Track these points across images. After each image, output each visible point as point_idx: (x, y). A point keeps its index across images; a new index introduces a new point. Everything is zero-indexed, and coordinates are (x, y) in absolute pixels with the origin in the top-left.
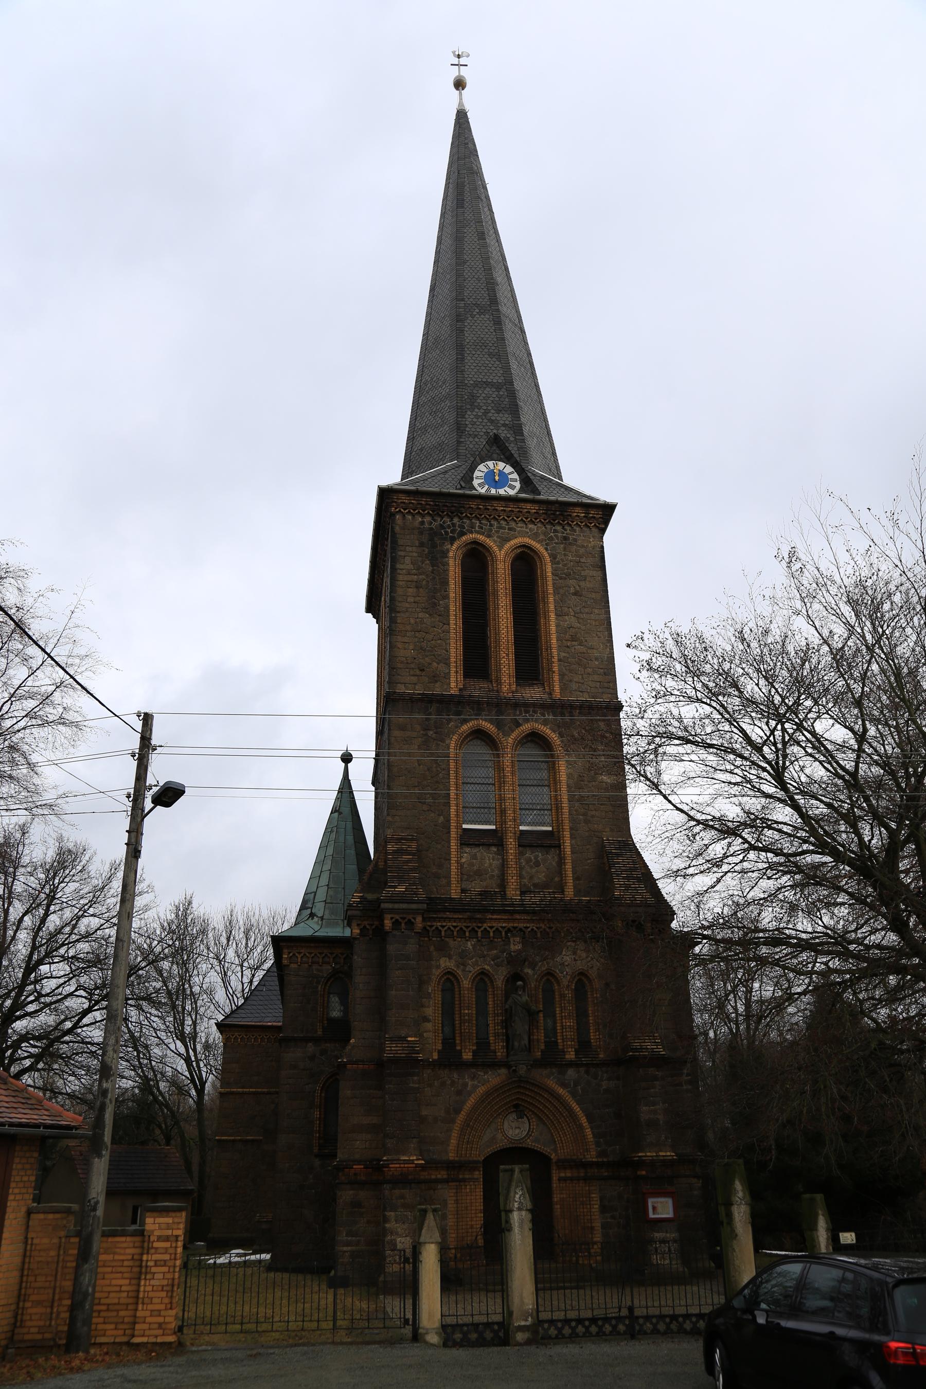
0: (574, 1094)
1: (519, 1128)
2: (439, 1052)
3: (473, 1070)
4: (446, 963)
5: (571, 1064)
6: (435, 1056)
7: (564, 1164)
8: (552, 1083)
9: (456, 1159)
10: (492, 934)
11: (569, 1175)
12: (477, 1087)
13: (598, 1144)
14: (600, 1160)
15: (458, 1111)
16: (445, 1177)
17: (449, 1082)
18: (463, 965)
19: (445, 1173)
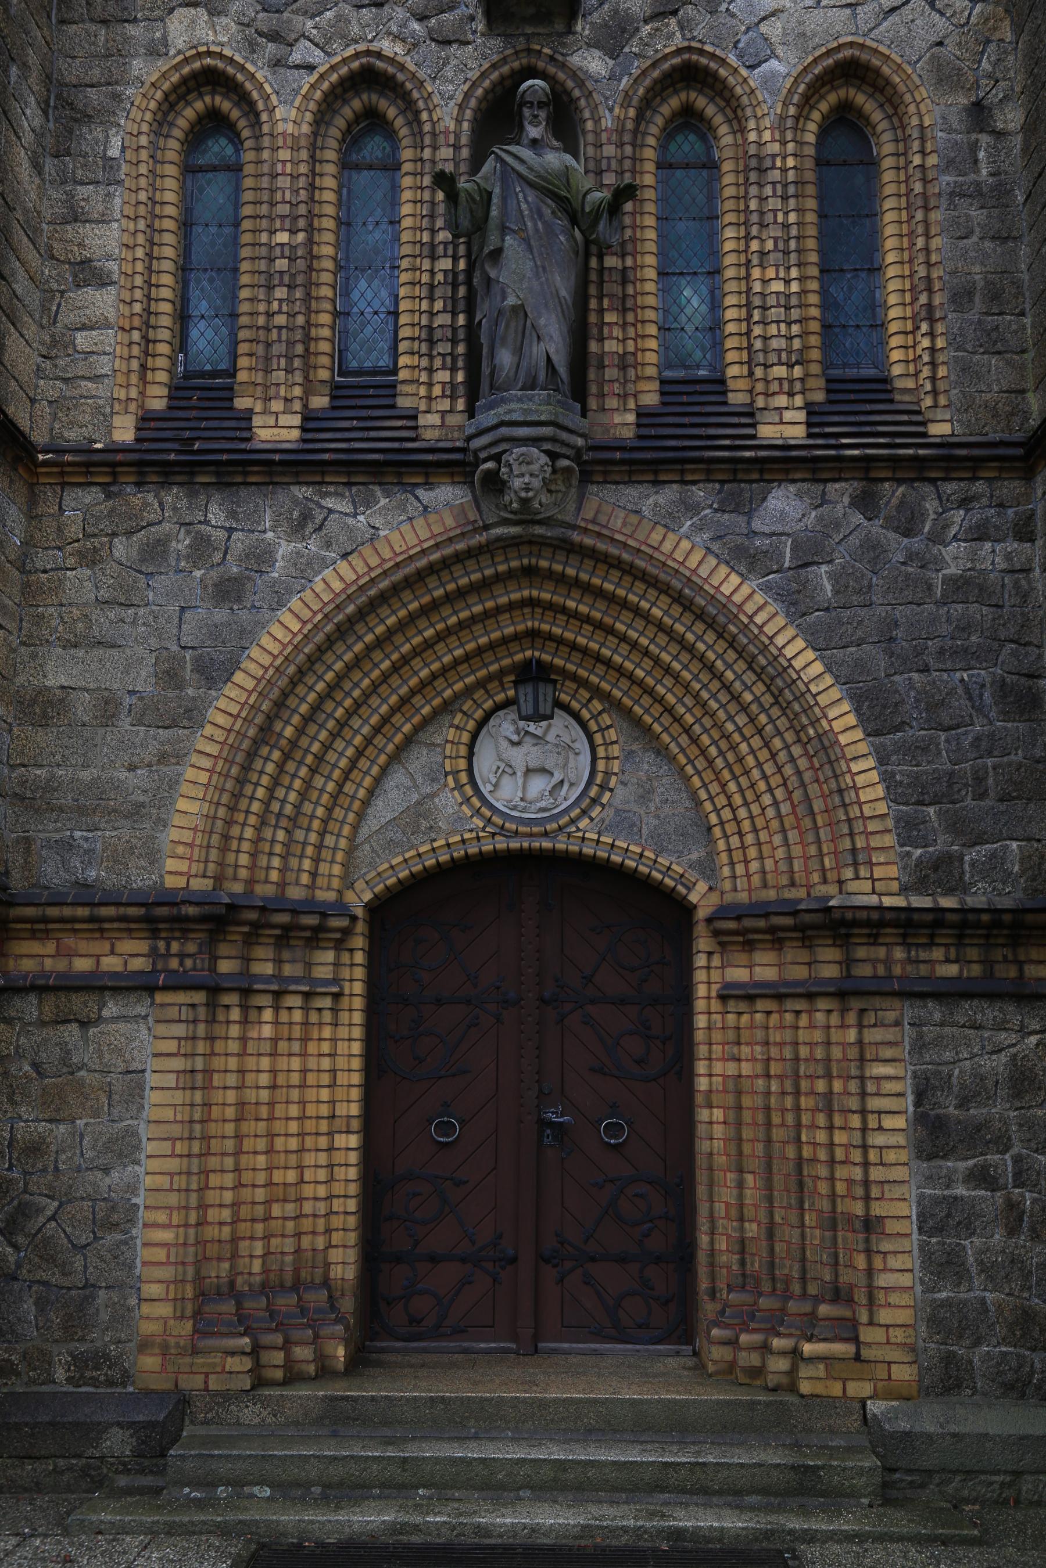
0: (795, 602)
1: (543, 771)
2: (146, 419)
3: (302, 492)
5: (782, 465)
6: (124, 431)
7: (747, 927)
9: (199, 884)
11: (767, 973)
13: (909, 830)
14: (920, 902)
15: (215, 672)
16: (138, 964)
17: (182, 543)
18: (274, 37)
19: (142, 946)
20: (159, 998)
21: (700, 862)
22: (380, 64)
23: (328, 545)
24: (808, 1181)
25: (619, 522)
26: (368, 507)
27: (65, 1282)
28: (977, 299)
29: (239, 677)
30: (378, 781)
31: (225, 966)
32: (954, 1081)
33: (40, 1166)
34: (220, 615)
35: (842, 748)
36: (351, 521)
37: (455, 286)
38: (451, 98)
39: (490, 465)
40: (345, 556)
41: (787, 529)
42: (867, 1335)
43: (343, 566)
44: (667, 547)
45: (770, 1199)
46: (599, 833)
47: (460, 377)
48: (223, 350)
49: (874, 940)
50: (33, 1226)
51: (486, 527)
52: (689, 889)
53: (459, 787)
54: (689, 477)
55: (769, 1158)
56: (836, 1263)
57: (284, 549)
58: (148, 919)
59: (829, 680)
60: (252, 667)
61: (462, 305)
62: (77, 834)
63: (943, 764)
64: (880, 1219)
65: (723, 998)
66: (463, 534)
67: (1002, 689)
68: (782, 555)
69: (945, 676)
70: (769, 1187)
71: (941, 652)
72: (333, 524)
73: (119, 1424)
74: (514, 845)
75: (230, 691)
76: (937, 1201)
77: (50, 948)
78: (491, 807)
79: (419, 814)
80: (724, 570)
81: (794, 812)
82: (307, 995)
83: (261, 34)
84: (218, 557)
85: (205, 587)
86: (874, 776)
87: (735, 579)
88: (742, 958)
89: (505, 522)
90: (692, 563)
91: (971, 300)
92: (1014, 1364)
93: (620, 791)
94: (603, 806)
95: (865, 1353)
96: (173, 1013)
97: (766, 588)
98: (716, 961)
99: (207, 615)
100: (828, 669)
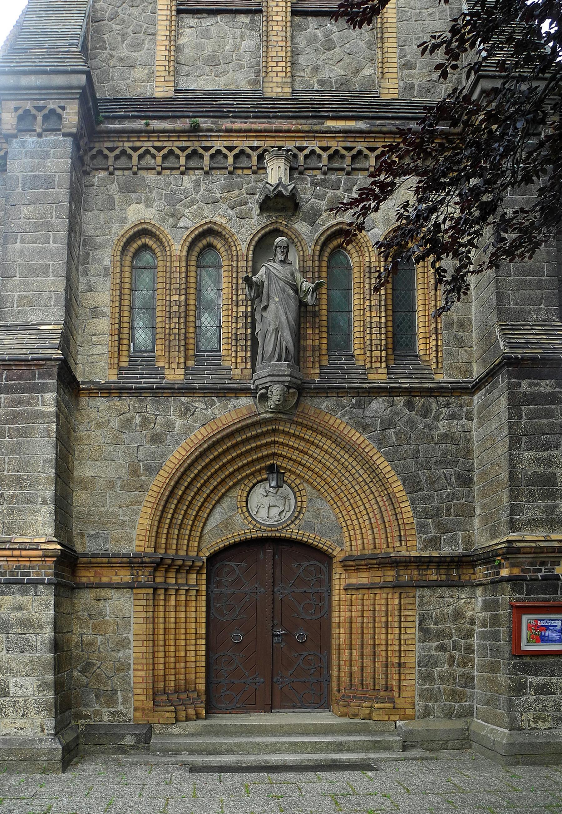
0: (380, 442)
4: (137, 213)
7: (353, 564)
8: (339, 422)
10: (231, 160)
12: (191, 429)
14: (426, 554)
17: (138, 420)
18: (173, 216)
20: (135, 591)
21: (338, 540)
22: (215, 227)
23: (196, 421)
24: (377, 652)
25: (313, 412)
26: (212, 406)
27: (106, 688)
28: (455, 326)
29: (162, 472)
30: (211, 510)
31: (158, 580)
32: (433, 616)
33: (93, 650)
34: (154, 449)
35: (397, 498)
36: (205, 412)
37: (246, 317)
38: (245, 241)
39: (263, 391)
40: (203, 425)
41: (379, 415)
42: (397, 700)
43: (202, 429)
44: (331, 422)
45: (362, 658)
46: (299, 530)
47: (249, 354)
48: (149, 342)
49: (406, 567)
50: (92, 670)
51: (259, 414)
52: (333, 550)
53: (243, 513)
54: (340, 395)
55: (362, 645)
56: (387, 678)
57: (178, 422)
58: (130, 563)
59: (393, 473)
60: (167, 468)
61: (249, 325)
62: (100, 532)
63: (435, 504)
64: (404, 663)
65: (346, 589)
66: (250, 417)
67: (458, 475)
68: (376, 425)
69: (437, 471)
70: (362, 654)
71: (436, 462)
72: (198, 413)
73: (130, 734)
74: (265, 534)
75: (158, 477)
76: (424, 656)
77: (92, 573)
78: (255, 520)
79: (227, 523)
80: (353, 431)
81: (377, 522)
82: (187, 591)
83: (167, 215)
84: (152, 426)
85: (147, 438)
86: (409, 509)
87: (358, 435)
88: (354, 575)
89: (267, 412)
90: (341, 428)
91: (452, 327)
92: (448, 707)
93: (307, 514)
94: (300, 520)
95: (396, 706)
96: (140, 596)
97: (370, 438)
98: (343, 576)
99: (148, 448)
100: (393, 469)
